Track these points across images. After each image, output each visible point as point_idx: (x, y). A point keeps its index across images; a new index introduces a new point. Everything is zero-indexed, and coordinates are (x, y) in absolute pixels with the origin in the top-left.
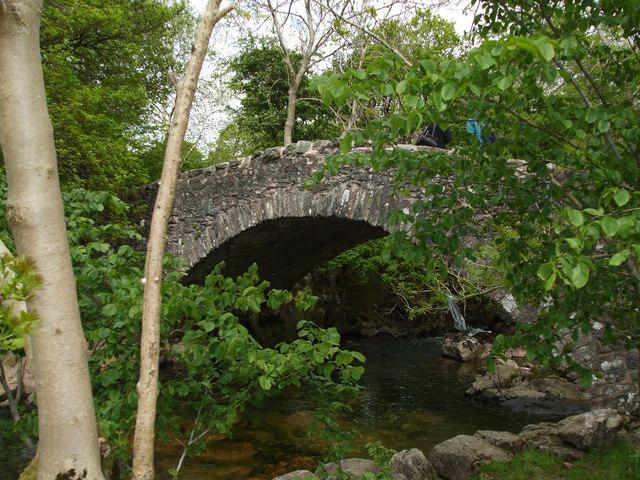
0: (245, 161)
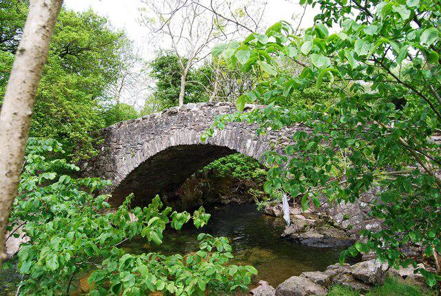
0: (158, 114)
